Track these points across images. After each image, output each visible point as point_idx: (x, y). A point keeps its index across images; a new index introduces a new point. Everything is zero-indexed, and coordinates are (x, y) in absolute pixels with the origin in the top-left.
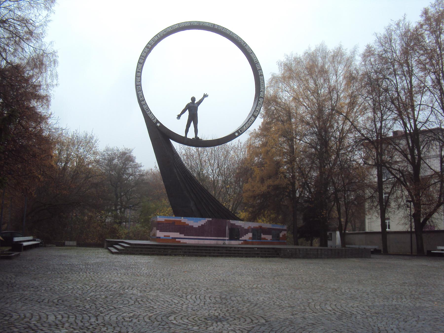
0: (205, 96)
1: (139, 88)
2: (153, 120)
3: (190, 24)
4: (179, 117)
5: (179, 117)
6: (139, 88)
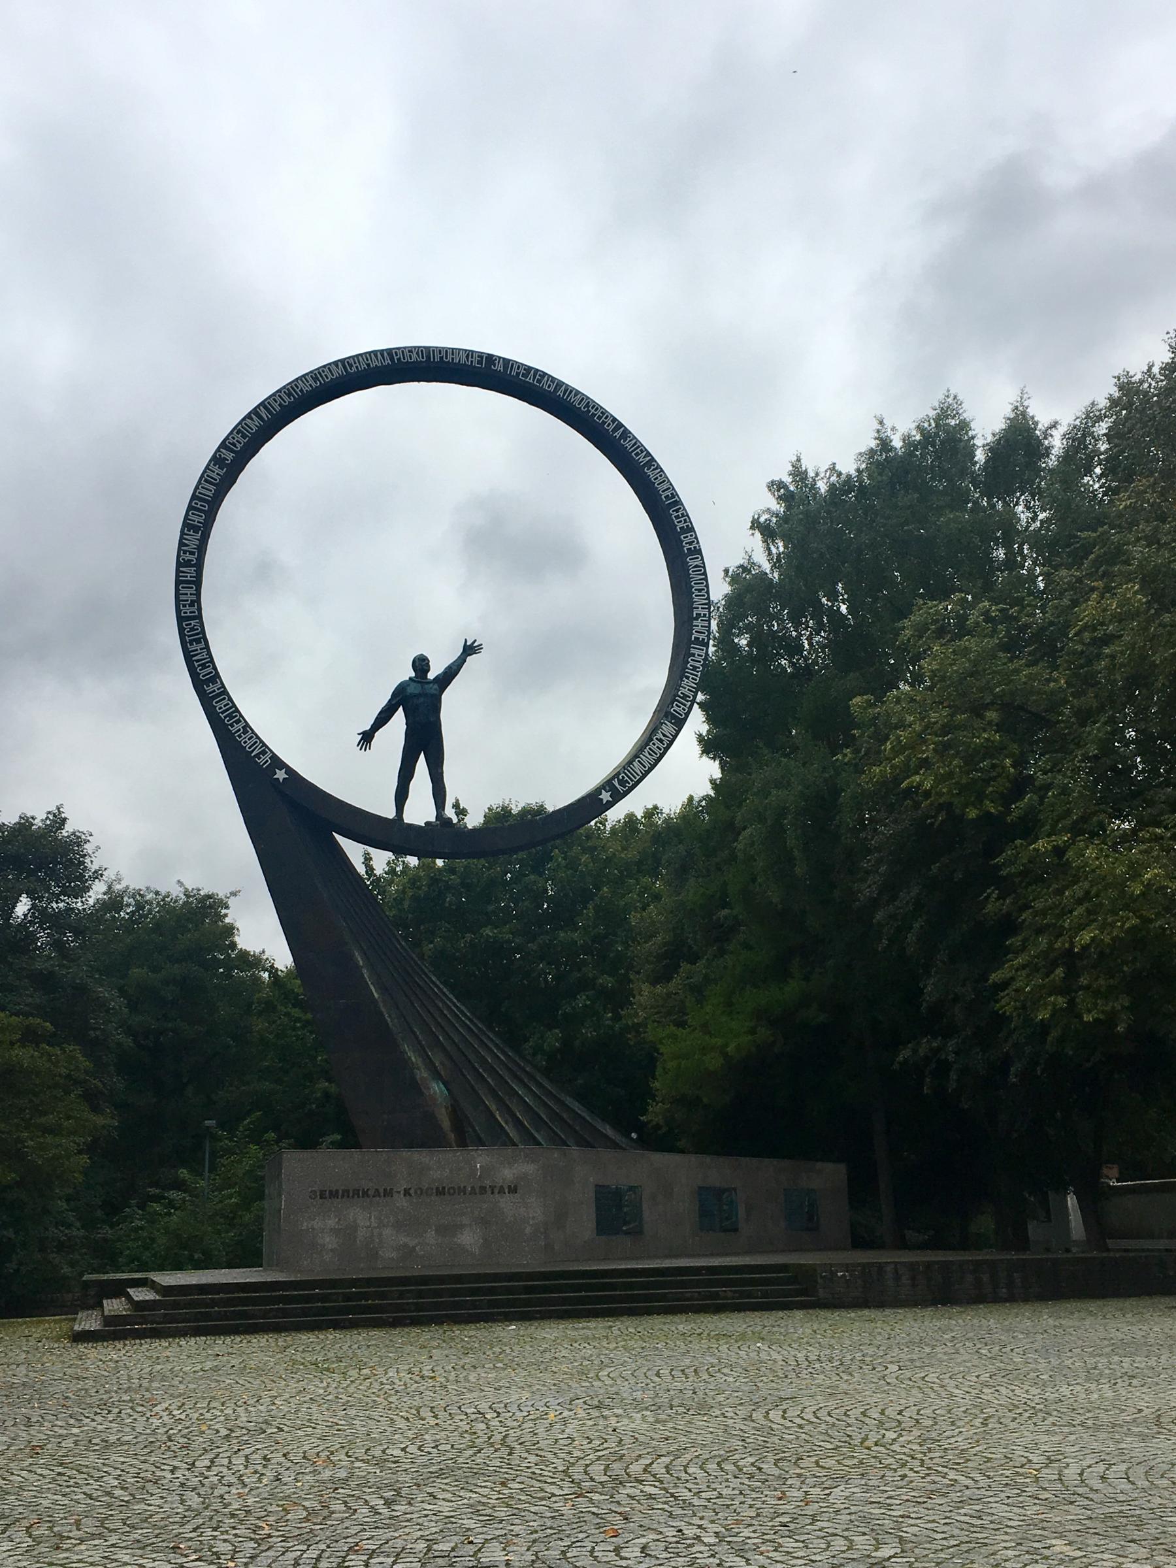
0: (470, 649)
1: (192, 629)
2: (258, 756)
3: (392, 358)
4: (367, 738)
5: (367, 738)
6: (192, 629)
